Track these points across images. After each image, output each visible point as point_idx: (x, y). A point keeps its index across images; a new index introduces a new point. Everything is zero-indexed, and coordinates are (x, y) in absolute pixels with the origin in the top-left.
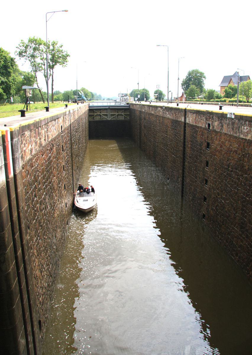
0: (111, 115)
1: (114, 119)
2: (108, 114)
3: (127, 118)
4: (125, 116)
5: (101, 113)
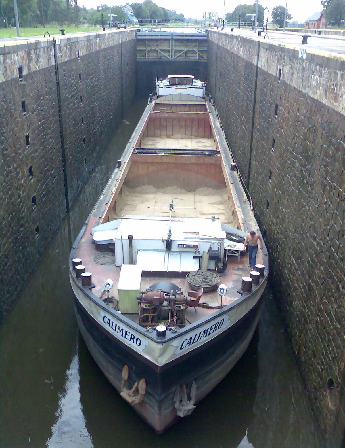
0: (176, 51)
1: (181, 58)
2: (170, 49)
3: (202, 57)
4: (200, 54)
5: (157, 46)
